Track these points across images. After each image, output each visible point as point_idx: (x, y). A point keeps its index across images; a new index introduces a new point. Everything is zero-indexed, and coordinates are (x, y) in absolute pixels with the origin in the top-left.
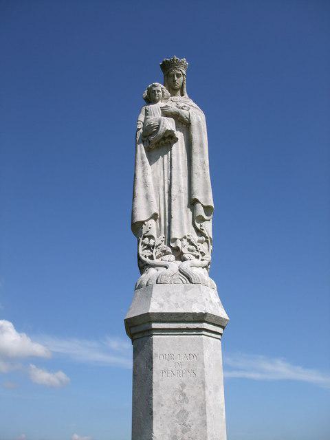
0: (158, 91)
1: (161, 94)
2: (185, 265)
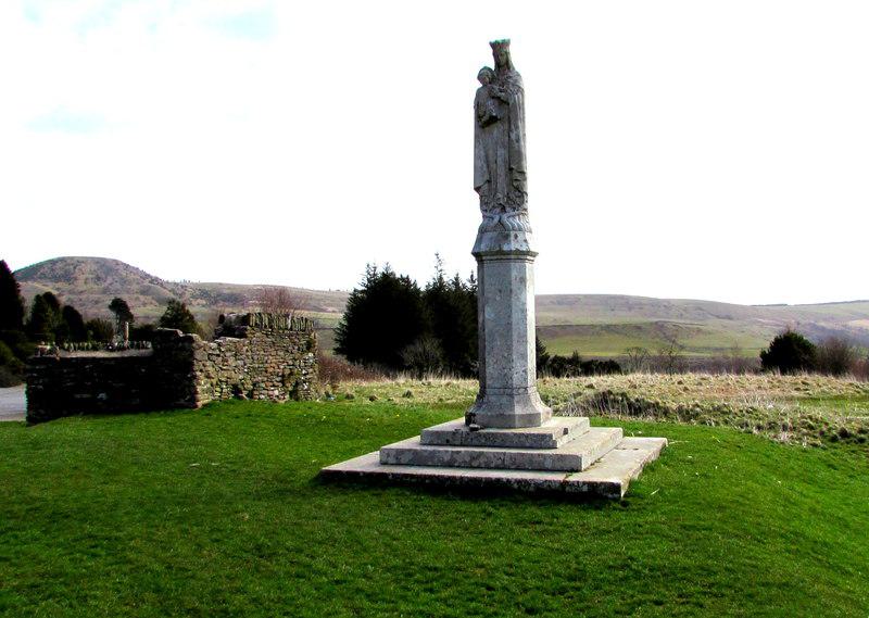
2: (505, 216)
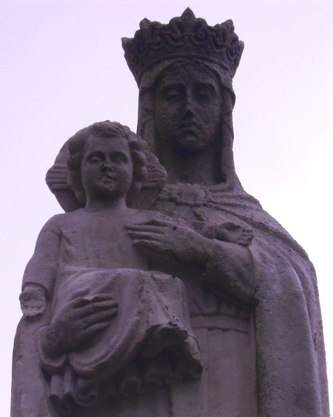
0: (117, 156)
1: (128, 168)
